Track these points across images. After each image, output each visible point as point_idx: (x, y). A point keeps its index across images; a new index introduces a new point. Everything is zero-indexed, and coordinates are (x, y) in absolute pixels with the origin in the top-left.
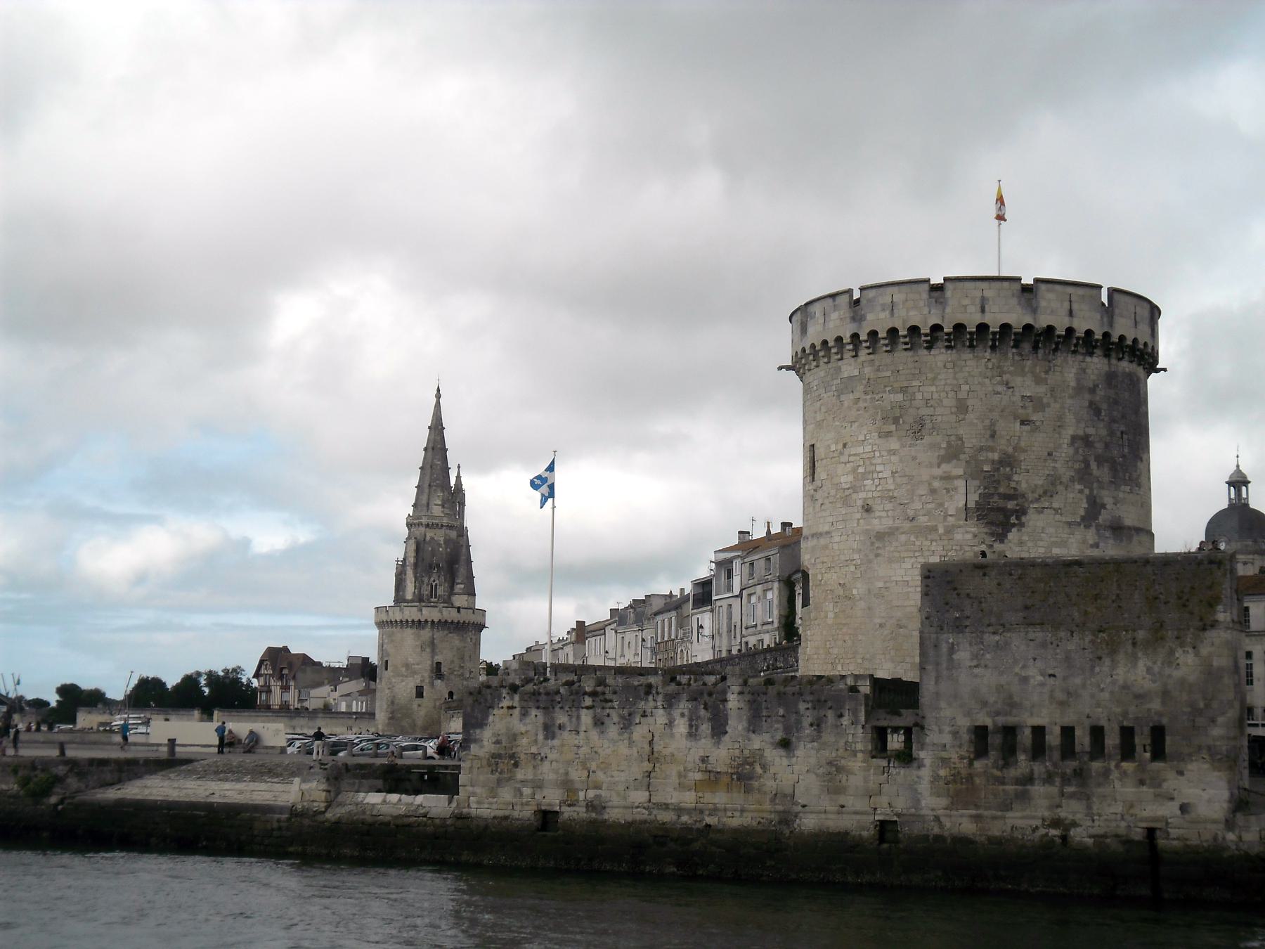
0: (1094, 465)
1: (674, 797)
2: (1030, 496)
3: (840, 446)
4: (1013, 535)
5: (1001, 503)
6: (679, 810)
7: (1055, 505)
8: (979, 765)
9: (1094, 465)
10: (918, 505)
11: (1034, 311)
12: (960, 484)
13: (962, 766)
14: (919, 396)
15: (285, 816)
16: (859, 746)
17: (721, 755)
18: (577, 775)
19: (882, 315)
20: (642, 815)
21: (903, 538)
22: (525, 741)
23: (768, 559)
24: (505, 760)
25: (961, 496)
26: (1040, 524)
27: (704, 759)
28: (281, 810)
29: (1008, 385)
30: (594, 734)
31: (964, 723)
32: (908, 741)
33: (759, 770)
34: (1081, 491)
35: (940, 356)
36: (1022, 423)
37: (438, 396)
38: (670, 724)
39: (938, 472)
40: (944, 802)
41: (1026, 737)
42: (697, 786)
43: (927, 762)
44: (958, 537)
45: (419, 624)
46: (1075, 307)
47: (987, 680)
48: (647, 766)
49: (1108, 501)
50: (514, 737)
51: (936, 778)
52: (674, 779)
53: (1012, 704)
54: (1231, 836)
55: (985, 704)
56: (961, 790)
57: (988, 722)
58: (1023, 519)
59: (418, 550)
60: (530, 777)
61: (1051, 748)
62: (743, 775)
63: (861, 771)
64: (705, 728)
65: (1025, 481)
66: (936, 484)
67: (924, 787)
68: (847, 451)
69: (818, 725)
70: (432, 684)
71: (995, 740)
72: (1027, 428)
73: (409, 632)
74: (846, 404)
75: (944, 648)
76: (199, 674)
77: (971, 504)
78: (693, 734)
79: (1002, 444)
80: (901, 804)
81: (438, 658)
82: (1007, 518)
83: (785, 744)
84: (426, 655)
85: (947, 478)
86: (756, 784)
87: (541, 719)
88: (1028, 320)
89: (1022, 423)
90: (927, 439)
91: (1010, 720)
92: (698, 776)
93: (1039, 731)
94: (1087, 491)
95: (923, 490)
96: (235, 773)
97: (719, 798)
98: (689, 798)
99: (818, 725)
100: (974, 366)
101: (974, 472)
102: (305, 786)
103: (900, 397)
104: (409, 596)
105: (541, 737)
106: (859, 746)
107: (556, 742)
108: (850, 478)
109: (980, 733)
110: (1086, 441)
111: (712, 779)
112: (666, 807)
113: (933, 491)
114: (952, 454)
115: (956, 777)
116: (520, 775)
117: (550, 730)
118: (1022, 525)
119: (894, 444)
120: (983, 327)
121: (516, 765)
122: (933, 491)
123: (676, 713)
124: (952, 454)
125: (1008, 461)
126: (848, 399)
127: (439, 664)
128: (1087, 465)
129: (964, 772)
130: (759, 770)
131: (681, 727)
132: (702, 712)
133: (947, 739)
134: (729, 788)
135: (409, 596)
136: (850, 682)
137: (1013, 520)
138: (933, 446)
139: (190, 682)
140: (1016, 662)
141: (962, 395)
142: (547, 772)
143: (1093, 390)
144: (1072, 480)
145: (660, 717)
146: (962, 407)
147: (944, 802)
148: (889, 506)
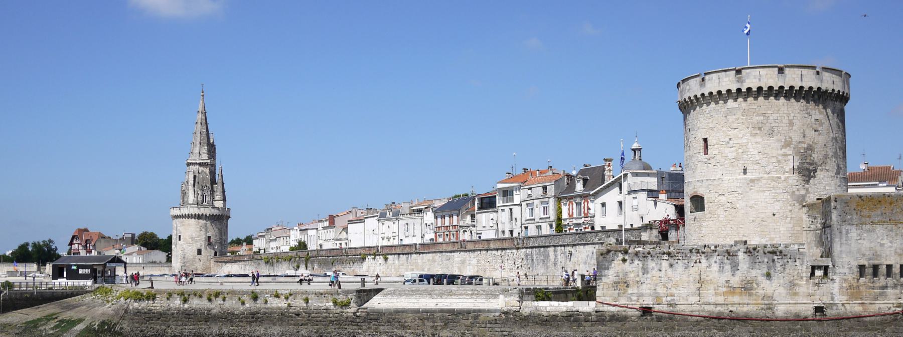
1: (712, 300)
2: (818, 164)
3: (727, 139)
5: (808, 166)
10: (771, 167)
11: (822, 81)
12: (791, 158)
13: (854, 282)
14: (771, 118)
15: (497, 314)
16: (804, 275)
17: (735, 281)
18: (661, 291)
19: (754, 80)
20: (696, 308)
21: (765, 182)
22: (632, 275)
23: (545, 188)
24: (622, 284)
25: (792, 162)
27: (727, 282)
28: (495, 311)
29: (809, 114)
30: (670, 271)
31: (855, 264)
33: (755, 286)
38: (709, 266)
40: (845, 298)
41: (883, 269)
42: (724, 294)
43: (837, 281)
44: (790, 182)
45: (198, 217)
47: (865, 244)
48: (698, 285)
51: (841, 288)
52: (712, 292)
53: (876, 255)
55: (864, 255)
56: (853, 292)
57: (866, 263)
60: (636, 292)
61: (895, 274)
62: (747, 288)
63: (805, 286)
64: (728, 267)
65: (816, 156)
66: (780, 158)
67: (836, 291)
68: (731, 142)
69: (784, 266)
71: (869, 271)
74: (731, 120)
75: (844, 232)
76: (27, 244)
77: (796, 167)
79: (808, 141)
80: (827, 300)
81: (208, 234)
83: (768, 275)
84: (203, 232)
85: (785, 155)
86: (754, 292)
87: (640, 265)
88: (819, 85)
90: (775, 138)
91: (876, 262)
92: (725, 289)
93: (889, 267)
95: (774, 160)
97: (736, 299)
98: (720, 299)
99: (784, 266)
100: (796, 107)
101: (797, 152)
102: (507, 299)
103: (762, 118)
104: (191, 201)
105: (641, 274)
106: (804, 275)
107: (649, 275)
108: (734, 154)
109: (862, 268)
111: (732, 290)
113: (779, 161)
114: (787, 144)
115: (851, 287)
116: (630, 291)
117: (645, 271)
119: (759, 139)
121: (627, 286)
122: (779, 161)
123: (713, 261)
124: (787, 144)
125: (810, 148)
126: (732, 118)
127: (209, 237)
129: (855, 285)
130: (755, 286)
131: (715, 267)
132: (726, 261)
133: (846, 270)
134: (740, 294)
135: (191, 201)
136: (713, 248)
138: (778, 141)
139: (23, 247)
140: (878, 237)
141: (791, 118)
142: (645, 289)
146: (791, 124)
147: (845, 298)
148: (756, 167)
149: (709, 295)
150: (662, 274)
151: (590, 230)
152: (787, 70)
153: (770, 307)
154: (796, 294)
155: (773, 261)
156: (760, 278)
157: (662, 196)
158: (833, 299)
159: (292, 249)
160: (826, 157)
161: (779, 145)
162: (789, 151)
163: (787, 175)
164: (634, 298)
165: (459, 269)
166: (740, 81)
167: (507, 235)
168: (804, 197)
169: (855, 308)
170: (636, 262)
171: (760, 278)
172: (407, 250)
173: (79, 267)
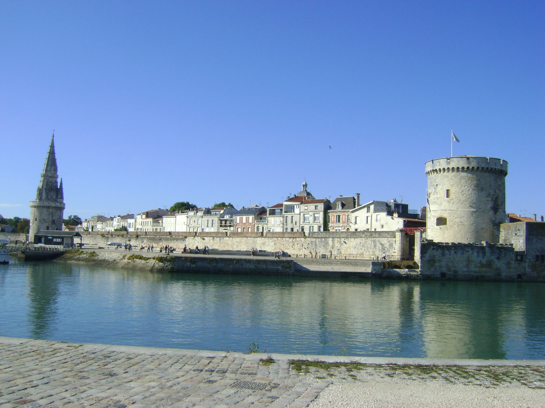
1: (473, 269)
6: (475, 272)
8: (537, 263)
17: (484, 261)
25: (490, 205)
27: (481, 261)
31: (534, 254)
32: (517, 258)
35: (487, 174)
37: (53, 136)
38: (473, 253)
39: (486, 199)
40: (531, 270)
45: (48, 207)
50: (434, 256)
51: (529, 265)
54: (194, 266)
59: (47, 184)
62: (489, 264)
64: (481, 254)
69: (505, 254)
70: (52, 226)
73: (45, 209)
78: (478, 256)
81: (54, 218)
83: (498, 258)
85: (488, 201)
96: (324, 264)
97: (484, 269)
98: (477, 269)
99: (505, 254)
100: (451, 174)
101: (492, 200)
111: (482, 265)
112: (472, 271)
114: (489, 195)
116: (436, 264)
117: (443, 255)
124: (489, 195)
131: (475, 254)
133: (531, 257)
142: (443, 263)
145: (471, 252)
146: (490, 186)
147: (531, 270)
149: (473, 268)
150: (451, 257)
151: (345, 230)
153: (499, 274)
154: (510, 268)
155: (501, 252)
156: (495, 260)
157: (396, 215)
158: (525, 270)
159: (116, 230)
164: (438, 268)
165: (260, 247)
166: (448, 163)
167: (289, 230)
168: (494, 221)
169: (535, 274)
170: (439, 250)
171: (495, 260)
172: (220, 235)
173: (54, 237)
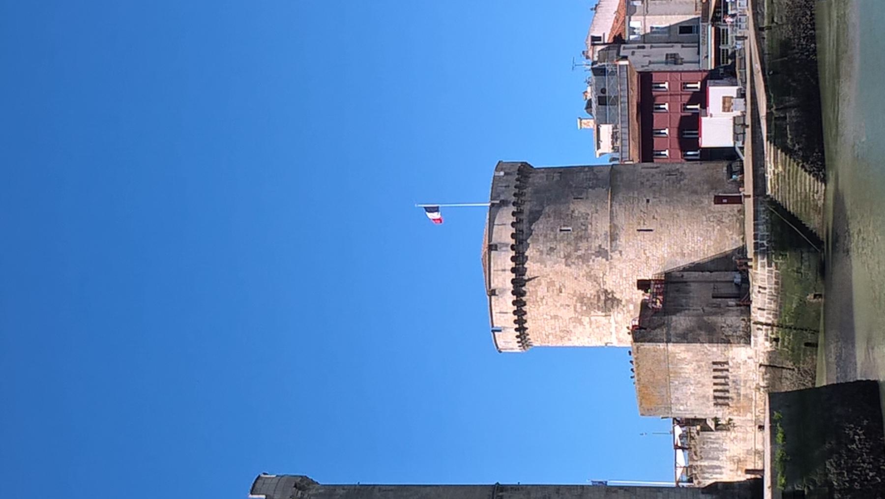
0: (579, 253)
4: (617, 296)
7: (601, 275)
9: (579, 253)
12: (592, 318)
25: (598, 317)
26: (611, 283)
34: (593, 261)
36: (561, 292)
39: (588, 326)
46: (500, 268)
49: (598, 242)
58: (609, 291)
65: (590, 290)
72: (563, 290)
77: (604, 314)
82: (609, 299)
85: (591, 323)
88: (510, 293)
89: (561, 292)
94: (593, 257)
101: (587, 313)
110: (567, 257)
118: (612, 292)
120: (513, 270)
125: (581, 299)
128: (580, 257)
137: (610, 296)
141: (549, 317)
143: (542, 252)
144: (588, 266)
146: (555, 317)
152: (493, 242)
160: (589, 276)
161: (580, 328)
162: (585, 320)
163: (612, 321)
